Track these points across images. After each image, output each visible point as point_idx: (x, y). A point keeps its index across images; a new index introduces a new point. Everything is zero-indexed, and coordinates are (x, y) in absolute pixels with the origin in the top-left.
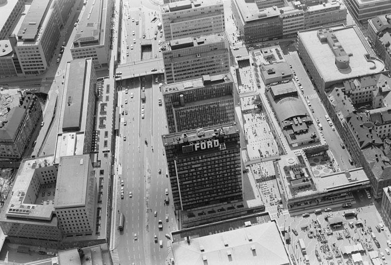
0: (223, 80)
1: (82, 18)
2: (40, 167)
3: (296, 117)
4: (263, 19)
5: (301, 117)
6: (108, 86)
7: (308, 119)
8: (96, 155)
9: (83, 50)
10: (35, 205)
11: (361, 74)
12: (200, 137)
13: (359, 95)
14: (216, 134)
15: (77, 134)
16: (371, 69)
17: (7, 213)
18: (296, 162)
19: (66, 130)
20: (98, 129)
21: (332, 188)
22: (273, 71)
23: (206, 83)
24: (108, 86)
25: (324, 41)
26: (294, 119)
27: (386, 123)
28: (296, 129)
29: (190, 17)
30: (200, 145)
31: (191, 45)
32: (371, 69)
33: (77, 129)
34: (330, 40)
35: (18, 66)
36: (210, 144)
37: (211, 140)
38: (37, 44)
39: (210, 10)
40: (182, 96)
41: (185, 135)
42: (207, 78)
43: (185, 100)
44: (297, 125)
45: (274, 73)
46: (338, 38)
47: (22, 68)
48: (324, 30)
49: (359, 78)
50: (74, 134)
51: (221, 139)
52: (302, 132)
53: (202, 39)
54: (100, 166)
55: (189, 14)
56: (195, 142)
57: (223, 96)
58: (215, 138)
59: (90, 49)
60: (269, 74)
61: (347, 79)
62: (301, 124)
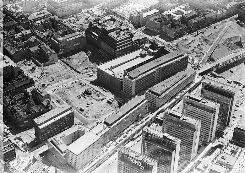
0: (173, 141)
2: (81, 130)
6: (149, 117)
8: (112, 142)
9: (148, 94)
10: (63, 143)
12: (136, 156)
14: (143, 160)
15: (107, 126)
17: (52, 139)
19: (105, 123)
20: (124, 132)
22: (224, 158)
23: (164, 137)
24: (149, 117)
30: (132, 160)
33: (109, 125)
35: (122, 88)
36: (136, 162)
37: (138, 161)
38: (133, 81)
39: (209, 108)
40: (150, 136)
41: (129, 151)
42: (166, 135)
47: (124, 88)
50: (106, 126)
54: (108, 148)
55: (197, 105)
56: (131, 157)
57: (160, 144)
58: (141, 161)
59: (149, 94)
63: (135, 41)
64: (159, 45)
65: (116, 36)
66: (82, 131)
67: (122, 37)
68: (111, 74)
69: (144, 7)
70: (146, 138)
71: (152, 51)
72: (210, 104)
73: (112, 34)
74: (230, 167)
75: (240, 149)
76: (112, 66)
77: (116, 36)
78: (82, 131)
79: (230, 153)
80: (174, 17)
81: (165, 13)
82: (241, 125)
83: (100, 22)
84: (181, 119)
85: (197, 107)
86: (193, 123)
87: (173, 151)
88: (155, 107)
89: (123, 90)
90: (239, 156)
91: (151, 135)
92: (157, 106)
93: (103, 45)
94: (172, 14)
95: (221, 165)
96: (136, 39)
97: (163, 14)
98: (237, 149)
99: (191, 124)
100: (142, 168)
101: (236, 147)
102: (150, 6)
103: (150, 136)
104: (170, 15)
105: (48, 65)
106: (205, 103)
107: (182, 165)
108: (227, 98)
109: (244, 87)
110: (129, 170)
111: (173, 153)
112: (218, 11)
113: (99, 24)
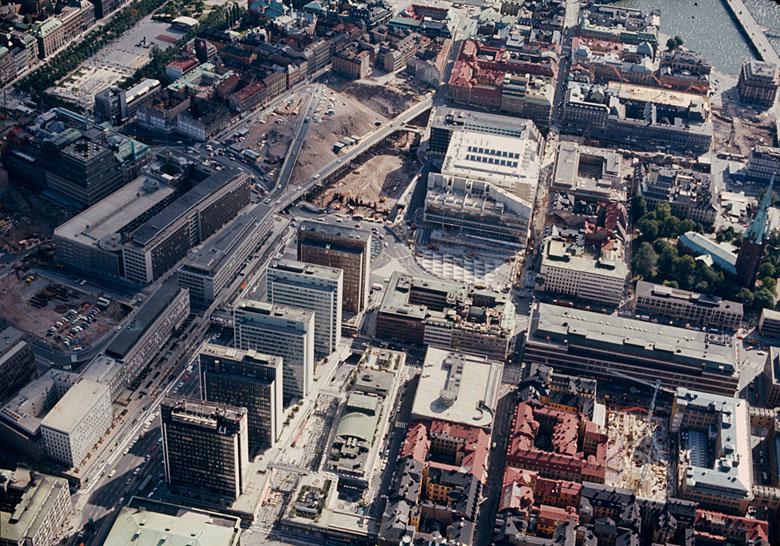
0: (266, 363)
1: (525, 25)
3: (353, 437)
4: (401, 316)
5: (359, 439)
7: (365, 445)
11: (455, 420)
13: (440, 443)
16: (474, 419)
18: (321, 485)
21: (241, 485)
23: (247, 358)
25: (447, 367)
26: (350, 439)
27: (443, 484)
28: (344, 450)
29: (298, 284)
31: (268, 313)
32: (474, 419)
34: (454, 369)
40: (217, 362)
42: (251, 353)
43: (221, 367)
44: (347, 446)
45: (369, 381)
46: (464, 371)
48: (456, 355)
49: (451, 423)
51: (221, 421)
52: (348, 456)
53: (279, 311)
55: (297, 279)
60: (363, 379)
61: (438, 420)
62: (353, 447)
63: (125, 159)
64: (181, 163)
65: (78, 155)
66: (63, 379)
67: (92, 154)
68: (90, 245)
69: (121, 76)
70: (211, 368)
71: (170, 178)
72: (322, 273)
73: (69, 151)
74: (384, 393)
75: (395, 354)
76: (88, 227)
77: (78, 155)
78: (63, 379)
79: (377, 367)
80: (197, 92)
81: (175, 85)
82: (388, 307)
83: (33, 128)
84: (272, 315)
85: (298, 284)
86: (298, 319)
87: (270, 383)
88: (202, 300)
89: (123, 276)
90: (395, 368)
91: (218, 359)
92: (206, 297)
93: (52, 179)
94: (191, 86)
95: (366, 394)
96: (125, 155)
97: (171, 87)
98: (391, 356)
99: (294, 323)
100: (222, 430)
101: (386, 351)
102: (134, 72)
103: (704, 328)
104: (187, 88)
105: (172, 300)
106: (311, 273)
107: (289, 410)
108: (352, 255)
109: (419, 542)
110: (190, 439)
111: (272, 385)
112: (289, 66)
113: (33, 133)
